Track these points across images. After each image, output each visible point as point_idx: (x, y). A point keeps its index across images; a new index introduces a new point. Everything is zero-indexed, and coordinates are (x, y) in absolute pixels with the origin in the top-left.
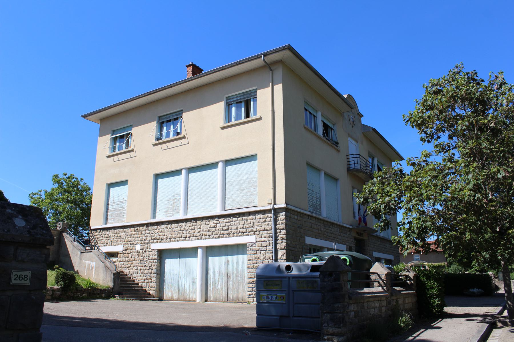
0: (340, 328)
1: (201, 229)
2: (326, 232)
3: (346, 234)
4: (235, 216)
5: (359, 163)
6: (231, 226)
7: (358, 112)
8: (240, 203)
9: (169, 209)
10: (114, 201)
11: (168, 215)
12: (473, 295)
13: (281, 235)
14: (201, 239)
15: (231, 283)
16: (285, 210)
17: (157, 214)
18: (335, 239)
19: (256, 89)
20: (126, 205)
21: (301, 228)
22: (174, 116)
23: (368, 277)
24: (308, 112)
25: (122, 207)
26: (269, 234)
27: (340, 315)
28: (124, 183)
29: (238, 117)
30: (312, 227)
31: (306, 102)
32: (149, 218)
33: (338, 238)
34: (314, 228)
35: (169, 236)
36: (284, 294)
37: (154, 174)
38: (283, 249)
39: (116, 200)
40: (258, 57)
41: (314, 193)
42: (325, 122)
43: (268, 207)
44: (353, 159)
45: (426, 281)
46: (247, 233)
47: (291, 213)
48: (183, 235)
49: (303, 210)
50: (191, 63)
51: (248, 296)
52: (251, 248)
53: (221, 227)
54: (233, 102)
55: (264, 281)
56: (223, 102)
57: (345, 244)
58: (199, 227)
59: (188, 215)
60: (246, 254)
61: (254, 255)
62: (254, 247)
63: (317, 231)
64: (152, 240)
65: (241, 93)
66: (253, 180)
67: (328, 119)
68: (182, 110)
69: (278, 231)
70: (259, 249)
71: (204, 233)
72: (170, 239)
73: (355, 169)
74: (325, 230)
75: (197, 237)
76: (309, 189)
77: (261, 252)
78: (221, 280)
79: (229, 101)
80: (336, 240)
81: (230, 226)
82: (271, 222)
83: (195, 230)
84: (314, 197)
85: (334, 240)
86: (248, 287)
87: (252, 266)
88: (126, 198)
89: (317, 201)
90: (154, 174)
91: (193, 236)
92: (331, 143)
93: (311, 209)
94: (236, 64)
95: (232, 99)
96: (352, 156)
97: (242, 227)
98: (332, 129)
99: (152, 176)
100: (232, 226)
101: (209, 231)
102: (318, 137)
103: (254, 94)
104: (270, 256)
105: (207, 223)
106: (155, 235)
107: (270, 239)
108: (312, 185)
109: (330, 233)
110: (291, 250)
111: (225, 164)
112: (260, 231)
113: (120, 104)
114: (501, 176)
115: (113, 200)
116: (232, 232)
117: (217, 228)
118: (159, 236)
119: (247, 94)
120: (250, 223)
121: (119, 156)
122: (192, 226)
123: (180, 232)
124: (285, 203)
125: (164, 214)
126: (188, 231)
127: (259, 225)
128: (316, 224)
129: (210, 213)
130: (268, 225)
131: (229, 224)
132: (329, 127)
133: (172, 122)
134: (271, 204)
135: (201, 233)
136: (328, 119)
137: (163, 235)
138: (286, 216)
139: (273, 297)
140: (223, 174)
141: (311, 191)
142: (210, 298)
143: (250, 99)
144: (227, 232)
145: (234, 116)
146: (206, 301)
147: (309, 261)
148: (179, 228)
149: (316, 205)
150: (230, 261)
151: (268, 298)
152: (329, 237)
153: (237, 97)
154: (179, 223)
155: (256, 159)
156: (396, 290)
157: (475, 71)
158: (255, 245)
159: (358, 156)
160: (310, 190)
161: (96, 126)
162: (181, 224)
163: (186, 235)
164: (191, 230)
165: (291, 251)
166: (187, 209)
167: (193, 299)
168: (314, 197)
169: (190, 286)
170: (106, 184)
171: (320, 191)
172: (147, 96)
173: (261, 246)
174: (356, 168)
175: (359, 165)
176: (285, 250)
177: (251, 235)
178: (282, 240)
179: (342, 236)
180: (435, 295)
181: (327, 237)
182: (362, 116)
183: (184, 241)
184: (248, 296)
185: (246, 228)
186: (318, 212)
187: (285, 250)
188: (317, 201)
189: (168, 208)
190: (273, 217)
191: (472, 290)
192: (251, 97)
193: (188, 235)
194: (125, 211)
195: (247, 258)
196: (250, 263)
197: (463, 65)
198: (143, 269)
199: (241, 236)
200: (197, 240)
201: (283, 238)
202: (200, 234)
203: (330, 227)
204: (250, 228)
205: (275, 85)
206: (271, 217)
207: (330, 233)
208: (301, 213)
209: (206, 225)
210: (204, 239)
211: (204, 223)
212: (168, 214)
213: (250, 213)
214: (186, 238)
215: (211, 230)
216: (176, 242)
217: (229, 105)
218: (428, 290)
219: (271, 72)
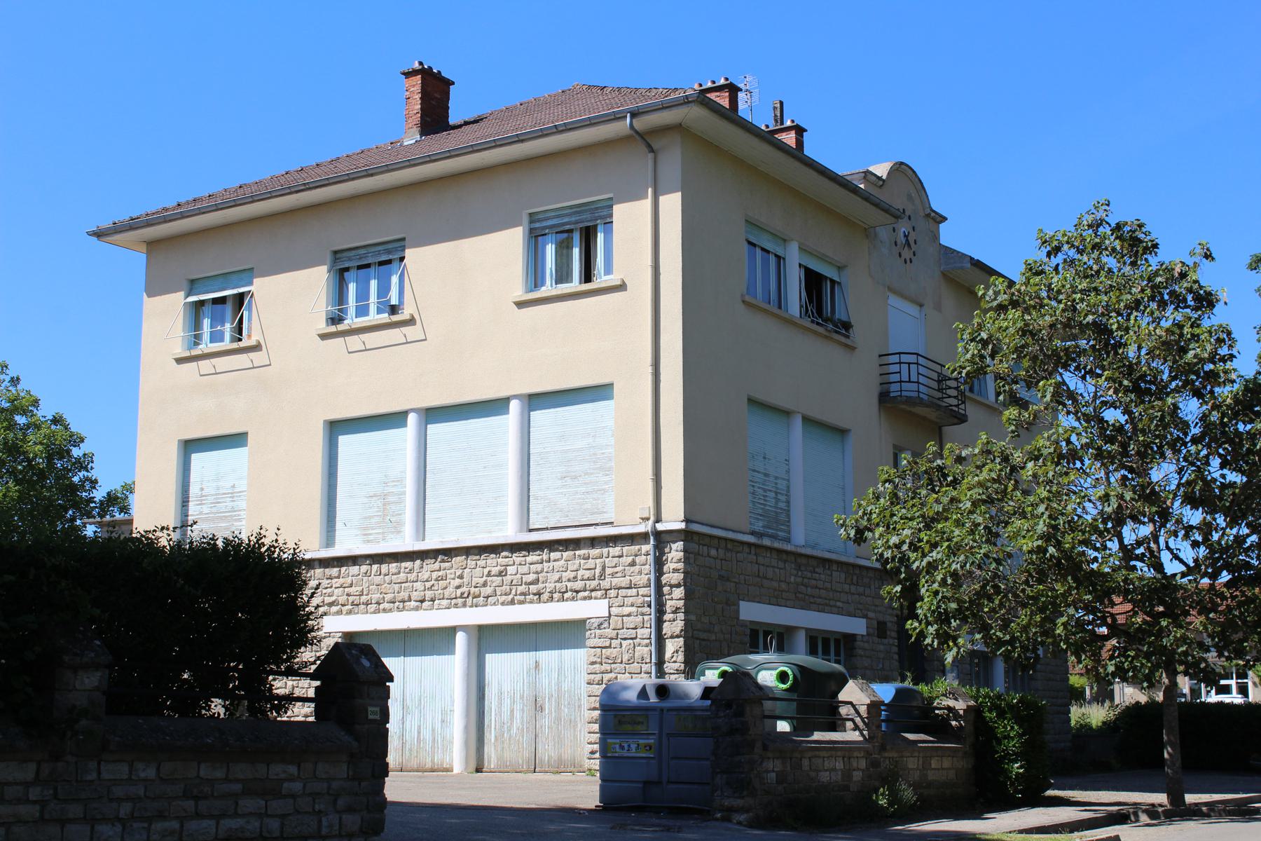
1: (465, 580)
2: (802, 585)
4: (556, 546)
5: (914, 378)
7: (929, 210)
9: (373, 521)
11: (371, 537)
13: (672, 599)
14: (464, 605)
15: (546, 721)
18: (832, 603)
19: (611, 199)
21: (728, 580)
22: (379, 253)
23: (834, 707)
24: (758, 251)
25: (229, 508)
26: (642, 596)
28: (235, 440)
30: (761, 574)
32: (317, 546)
33: (839, 601)
34: (766, 578)
37: (325, 421)
38: (678, 637)
41: (772, 479)
43: (641, 529)
45: (995, 722)
46: (588, 592)
47: (701, 542)
48: (415, 595)
49: (733, 531)
50: (416, 66)
51: (589, 755)
53: (519, 576)
54: (547, 231)
58: (457, 575)
59: (427, 541)
60: (585, 647)
61: (604, 650)
62: (605, 628)
63: (775, 584)
64: (326, 607)
65: (571, 207)
66: (603, 453)
68: (403, 239)
69: (666, 589)
70: (617, 634)
71: (473, 590)
72: (379, 603)
73: (901, 396)
74: (801, 579)
77: (623, 642)
79: (537, 225)
80: (835, 606)
81: (542, 572)
82: (647, 567)
83: (448, 581)
84: (770, 491)
86: (589, 733)
87: (598, 677)
88: (242, 485)
89: (777, 500)
90: (325, 421)
91: (441, 597)
93: (761, 524)
94: (555, 130)
96: (895, 359)
97: (574, 578)
98: (833, 282)
99: (320, 426)
100: (547, 572)
101: (485, 585)
102: (790, 322)
103: (605, 213)
104: (645, 652)
106: (335, 594)
107: (646, 610)
108: (765, 458)
109: (816, 587)
110: (697, 639)
111: (526, 406)
112: (619, 589)
113: (215, 208)
114: (1111, 508)
115: (202, 489)
116: (548, 590)
117: (509, 578)
118: (345, 597)
119: (586, 211)
120: (593, 566)
121: (215, 361)
122: (439, 570)
124: (682, 517)
125: (357, 535)
126: (428, 585)
127: (617, 573)
128: (773, 567)
130: (640, 573)
132: (826, 278)
133: (372, 270)
134: (648, 519)
135: (464, 589)
136: (822, 258)
137: (357, 593)
138: (685, 551)
140: (522, 433)
141: (761, 476)
142: (489, 762)
143: (595, 227)
144: (533, 588)
145: (551, 269)
147: (714, 674)
148: (402, 574)
149: (776, 512)
150: (543, 665)
151: (622, 747)
153: (558, 216)
154: (401, 562)
157: (1138, 220)
158: (606, 625)
159: (912, 359)
160: (758, 472)
161: (137, 261)
162: (409, 564)
163: (422, 593)
166: (424, 522)
167: (442, 764)
168: (770, 491)
169: (433, 730)
171: (788, 472)
172: (299, 194)
173: (621, 627)
174: (904, 393)
175: (914, 387)
176: (682, 639)
177: (596, 598)
178: (675, 612)
179: (854, 594)
180: (1015, 753)
181: (807, 597)
182: (939, 219)
183: (417, 610)
184: (589, 755)
185: (582, 580)
186: (781, 531)
187: (682, 639)
188: (777, 500)
189: (370, 517)
190: (652, 553)
192: (598, 222)
193: (429, 594)
194: (240, 523)
195: (586, 658)
196: (593, 671)
198: (300, 685)
199: (571, 600)
200: (452, 609)
201: (677, 608)
203: (817, 570)
204: (594, 579)
205: (663, 195)
207: (816, 587)
209: (478, 569)
210: (471, 606)
211: (471, 563)
212: (370, 534)
213: (593, 542)
214: (422, 601)
215: (493, 582)
216: (395, 614)
218: (999, 742)
219: (651, 155)
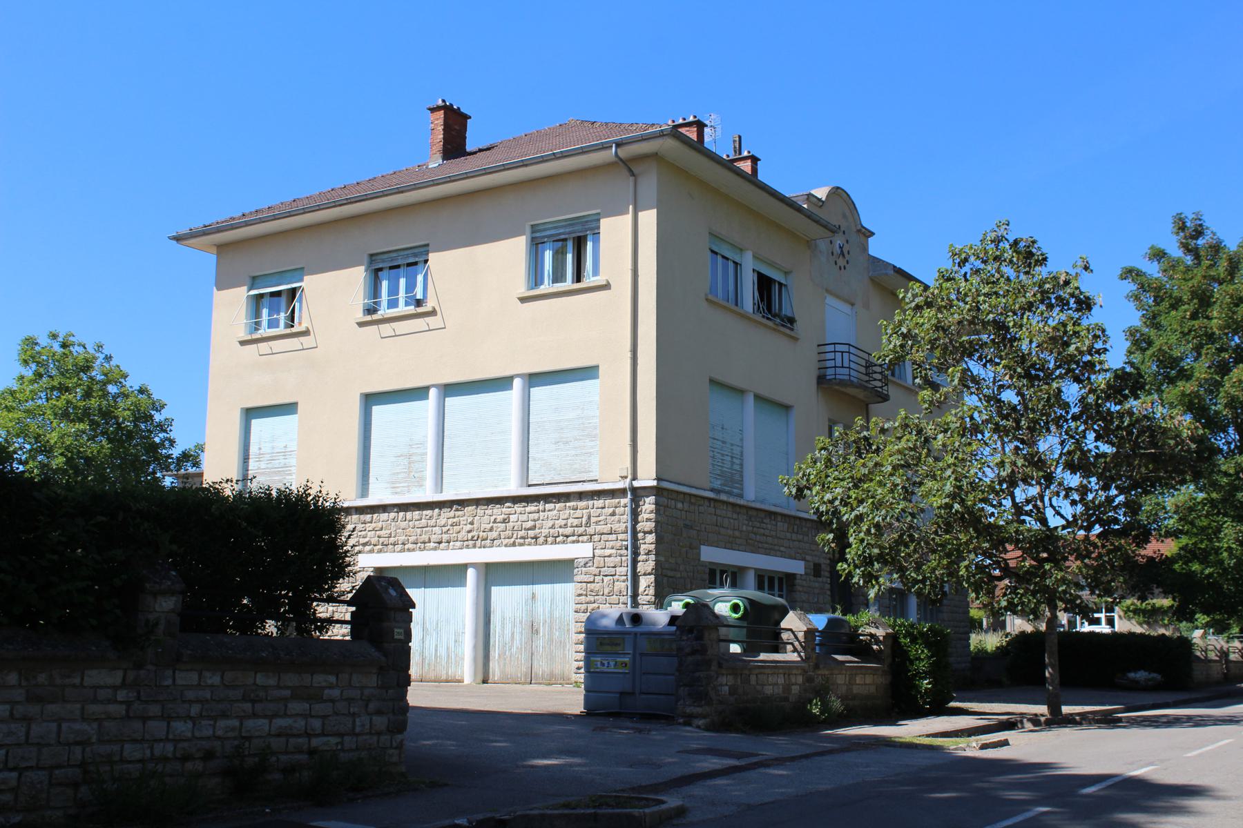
0: (701, 706)
2: (752, 532)
3: (808, 536)
5: (846, 364)
6: (540, 521)
8: (561, 470)
9: (400, 476)
10: (262, 452)
11: (398, 490)
12: (1136, 687)
13: (645, 543)
14: (474, 546)
15: (540, 642)
16: (655, 493)
17: (371, 486)
18: (776, 548)
19: (599, 214)
20: (293, 461)
21: (691, 528)
22: (408, 256)
23: (777, 634)
24: (719, 258)
25: (282, 465)
26: (621, 540)
27: (702, 688)
28: (288, 408)
29: (558, 276)
31: (712, 235)
32: (353, 495)
35: (402, 538)
36: (626, 660)
38: (649, 574)
39: (266, 449)
40: (605, 147)
42: (762, 272)
43: (620, 485)
44: (831, 356)
48: (434, 538)
49: (696, 488)
51: (576, 671)
52: (584, 569)
53: (519, 523)
54: (546, 240)
55: (598, 639)
56: (524, 237)
57: (803, 559)
60: (573, 581)
61: (589, 585)
63: (730, 532)
66: (590, 423)
67: (772, 265)
68: (427, 245)
69: (640, 535)
70: (600, 572)
71: (481, 534)
72: (404, 544)
75: (466, 543)
76: (715, 439)
78: (517, 637)
79: (538, 235)
80: (779, 550)
81: (538, 520)
82: (625, 516)
85: (771, 549)
87: (584, 607)
89: (733, 463)
92: (775, 324)
93: (719, 482)
95: (545, 230)
96: (831, 348)
98: (781, 284)
101: (491, 530)
102: (744, 316)
103: (593, 225)
105: (489, 512)
107: (624, 552)
109: (764, 535)
110: (666, 576)
114: (1005, 473)
115: (260, 449)
116: (543, 535)
117: (511, 524)
122: (454, 517)
123: (427, 529)
124: (654, 476)
126: (445, 529)
128: (729, 518)
129: (495, 489)
130: (619, 521)
131: (536, 516)
132: (775, 281)
133: (401, 270)
134: (626, 477)
135: (474, 533)
136: (772, 265)
138: (656, 504)
139: (609, 664)
141: (719, 443)
142: (494, 675)
144: (531, 533)
146: (485, 681)
149: (731, 473)
150: (538, 596)
152: (760, 545)
153: (555, 228)
155: (596, 377)
156: (836, 659)
158: (590, 564)
159: (845, 348)
162: (429, 512)
163: (440, 536)
164: (452, 525)
165: (665, 579)
166: (442, 477)
169: (448, 648)
170: (242, 408)
171: (742, 440)
175: (846, 371)
176: (653, 576)
177: (582, 542)
178: (647, 554)
184: (576, 671)
185: (572, 527)
188: (733, 463)
189: (398, 473)
190: (629, 505)
191: (1132, 675)
192: (588, 232)
193: (445, 537)
194: (290, 477)
195: (574, 591)
197: (1008, 225)
198: (339, 610)
201: (649, 551)
202: (473, 537)
203: (765, 521)
205: (641, 211)
206: (625, 506)
207: (764, 535)
208: (690, 495)
209: (486, 517)
210: (480, 547)
212: (398, 487)
214: (440, 543)
215: (497, 527)
216: (418, 553)
217: (537, 244)
218: (912, 663)
219: (632, 179)
